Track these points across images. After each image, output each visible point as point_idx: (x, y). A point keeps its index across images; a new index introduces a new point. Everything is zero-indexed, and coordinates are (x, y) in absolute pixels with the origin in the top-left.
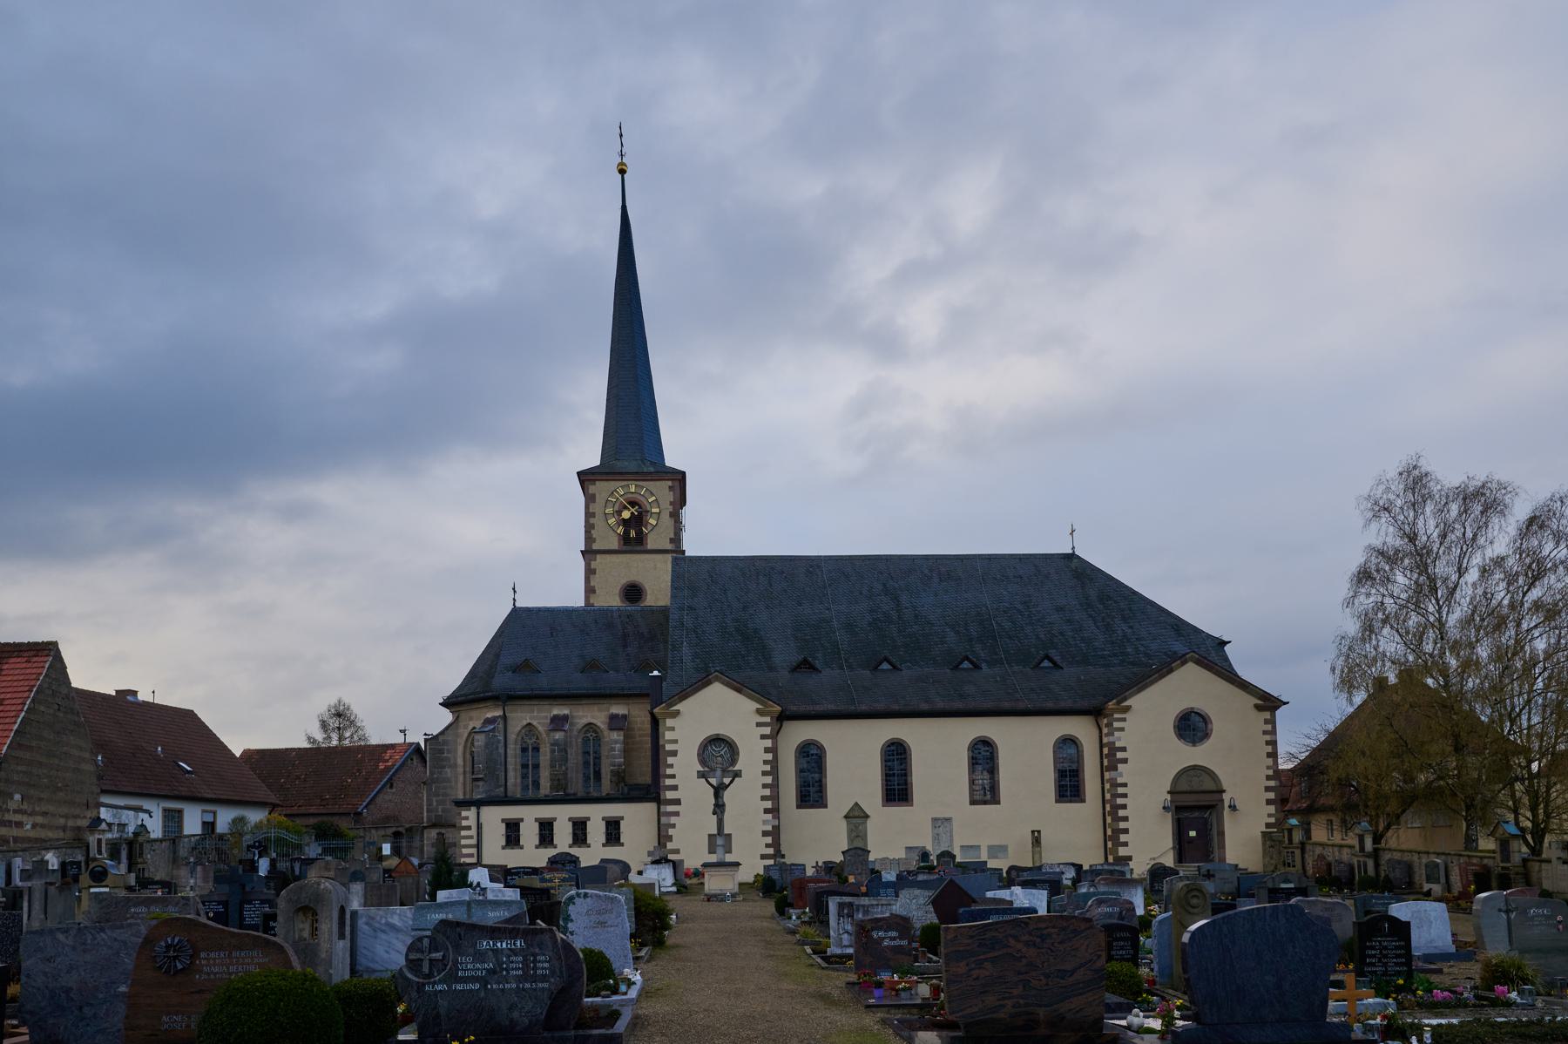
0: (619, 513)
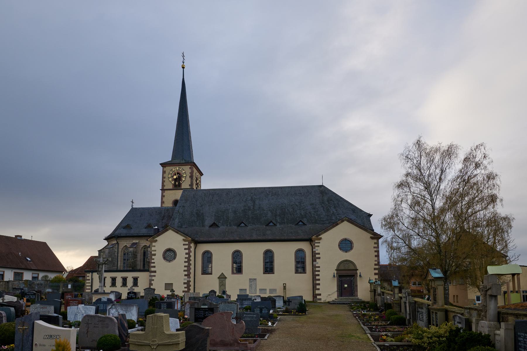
0: (173, 177)
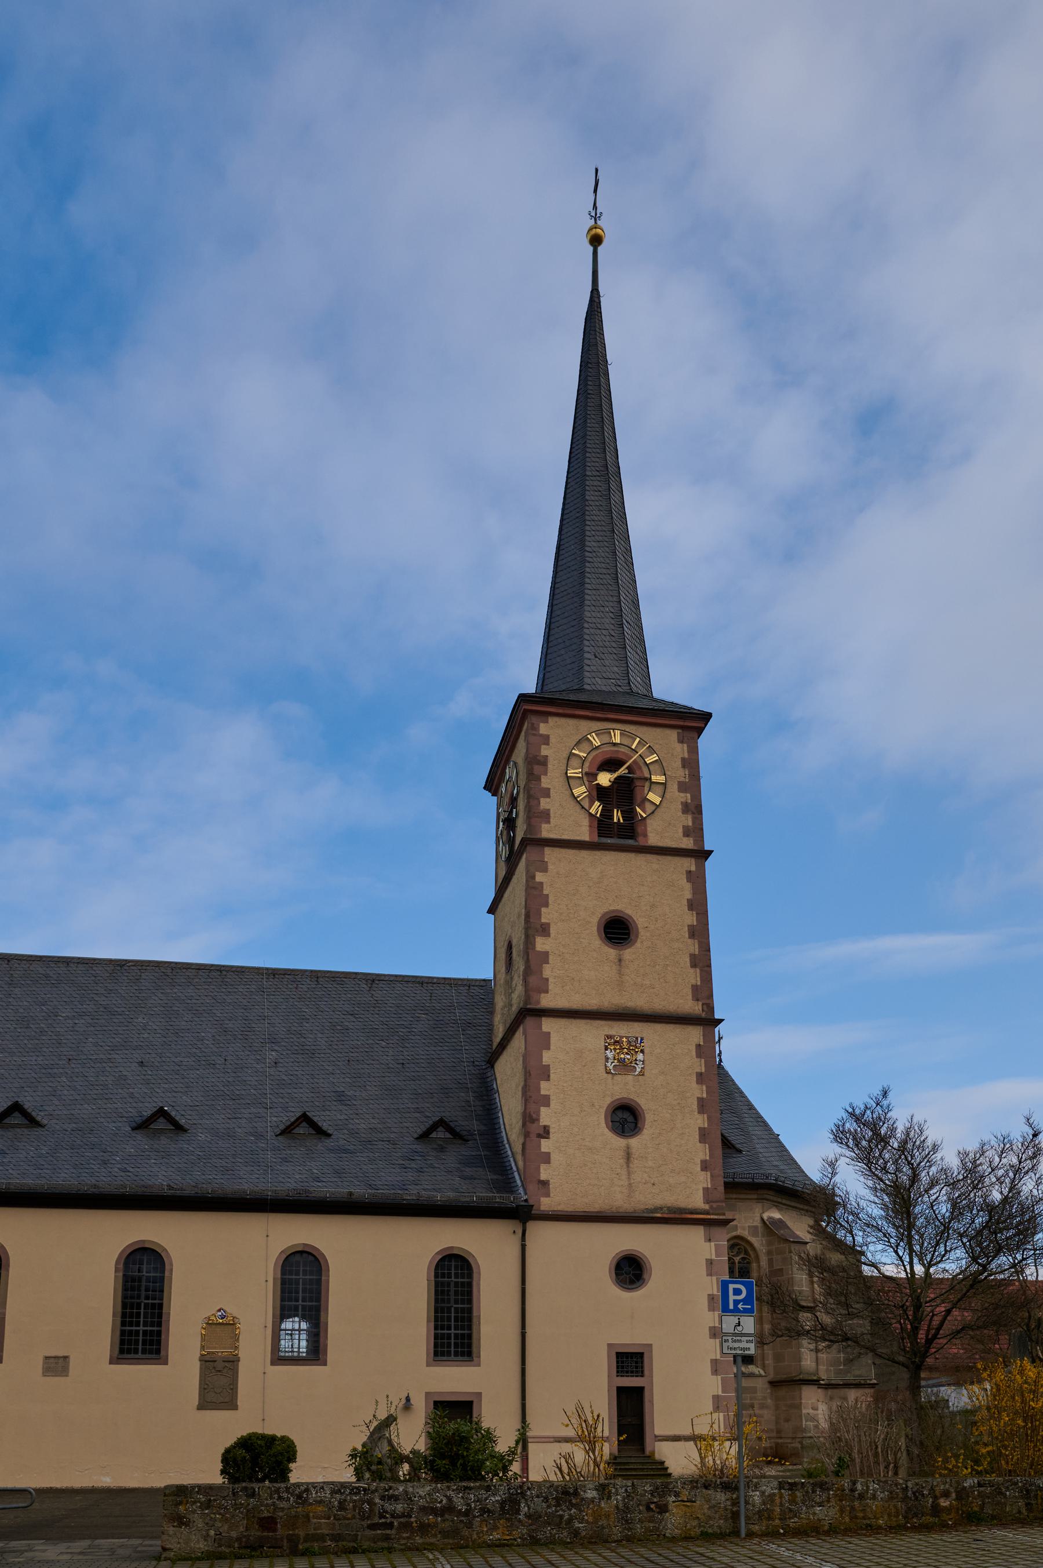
0: (592, 776)
